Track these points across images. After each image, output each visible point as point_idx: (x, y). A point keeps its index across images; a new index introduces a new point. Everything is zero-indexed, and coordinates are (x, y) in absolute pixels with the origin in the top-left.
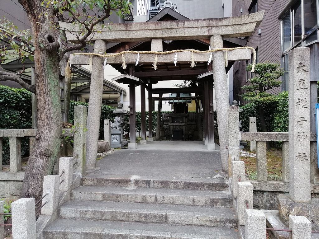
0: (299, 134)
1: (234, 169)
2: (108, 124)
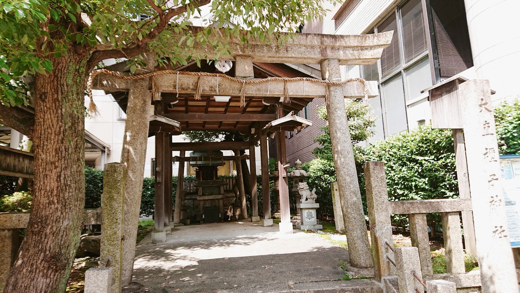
0: (492, 199)
1: (404, 261)
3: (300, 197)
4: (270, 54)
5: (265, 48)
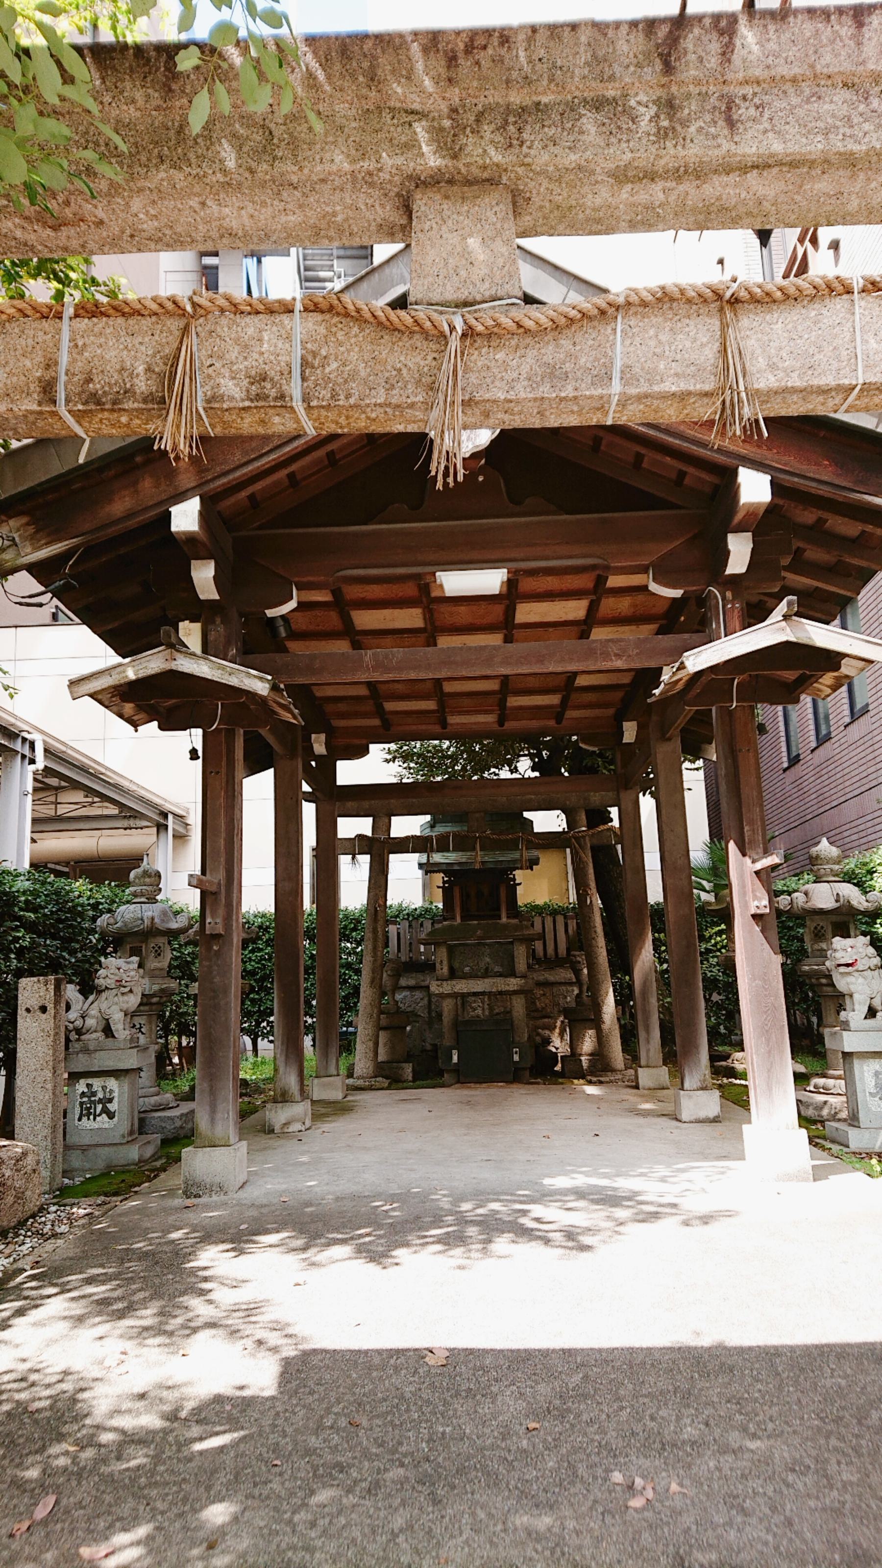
2: (43, 1009)
3: (840, 1000)
4: (621, 155)
5: (589, 122)
